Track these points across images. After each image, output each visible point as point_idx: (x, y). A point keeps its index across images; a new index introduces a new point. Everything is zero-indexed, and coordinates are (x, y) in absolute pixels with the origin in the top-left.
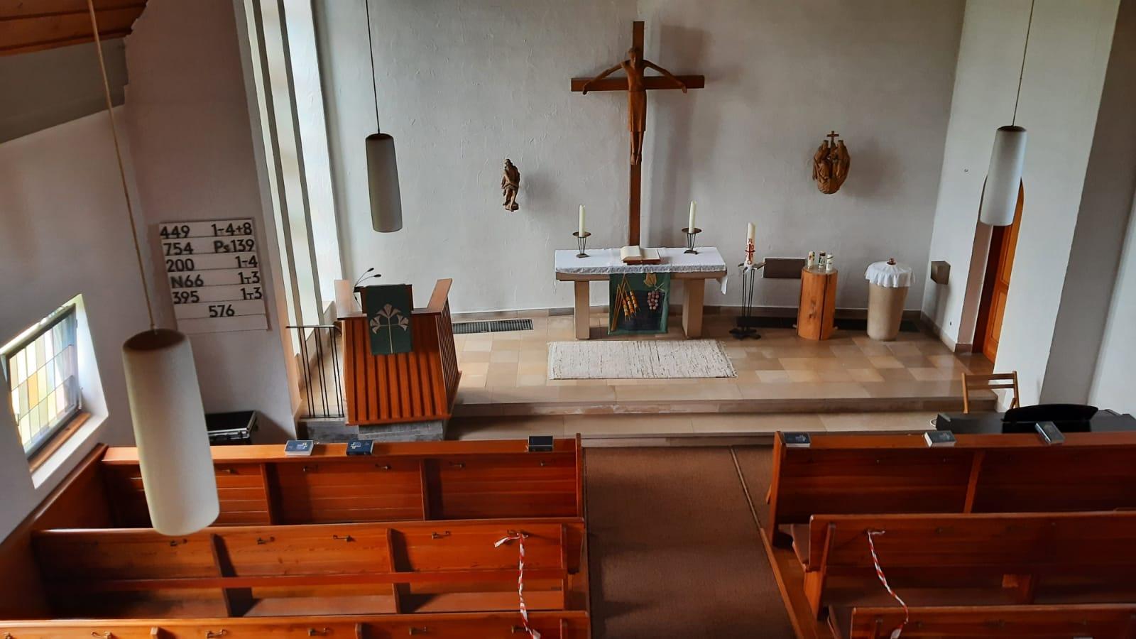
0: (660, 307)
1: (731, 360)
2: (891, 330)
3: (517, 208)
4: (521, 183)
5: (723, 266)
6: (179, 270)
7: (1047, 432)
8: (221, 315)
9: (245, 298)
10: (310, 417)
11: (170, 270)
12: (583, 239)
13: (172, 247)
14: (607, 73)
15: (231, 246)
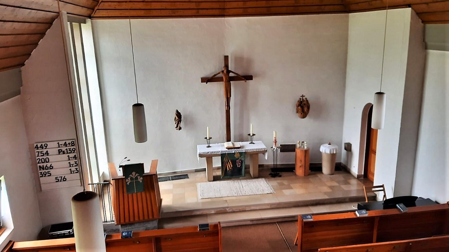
0: (241, 166)
1: (272, 186)
2: (331, 170)
3: (181, 129)
5: (265, 148)
6: (42, 163)
8: (61, 181)
9: (71, 173)
11: (39, 163)
12: (209, 140)
13: (40, 153)
14: (215, 75)
15: (66, 151)
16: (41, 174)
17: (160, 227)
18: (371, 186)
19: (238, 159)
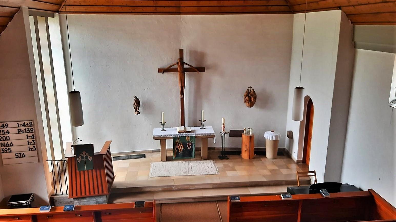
0: (192, 148)
1: (217, 167)
2: (274, 155)
3: (139, 113)
4: (141, 104)
6: (4, 140)
7: (324, 193)
8: (20, 157)
10: (55, 195)
12: (163, 124)
14: (171, 66)
15: (24, 131)
16: (2, 150)
17: (110, 201)
18: (307, 171)
19: (188, 142)
